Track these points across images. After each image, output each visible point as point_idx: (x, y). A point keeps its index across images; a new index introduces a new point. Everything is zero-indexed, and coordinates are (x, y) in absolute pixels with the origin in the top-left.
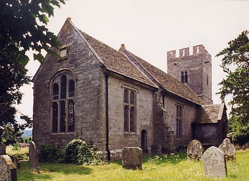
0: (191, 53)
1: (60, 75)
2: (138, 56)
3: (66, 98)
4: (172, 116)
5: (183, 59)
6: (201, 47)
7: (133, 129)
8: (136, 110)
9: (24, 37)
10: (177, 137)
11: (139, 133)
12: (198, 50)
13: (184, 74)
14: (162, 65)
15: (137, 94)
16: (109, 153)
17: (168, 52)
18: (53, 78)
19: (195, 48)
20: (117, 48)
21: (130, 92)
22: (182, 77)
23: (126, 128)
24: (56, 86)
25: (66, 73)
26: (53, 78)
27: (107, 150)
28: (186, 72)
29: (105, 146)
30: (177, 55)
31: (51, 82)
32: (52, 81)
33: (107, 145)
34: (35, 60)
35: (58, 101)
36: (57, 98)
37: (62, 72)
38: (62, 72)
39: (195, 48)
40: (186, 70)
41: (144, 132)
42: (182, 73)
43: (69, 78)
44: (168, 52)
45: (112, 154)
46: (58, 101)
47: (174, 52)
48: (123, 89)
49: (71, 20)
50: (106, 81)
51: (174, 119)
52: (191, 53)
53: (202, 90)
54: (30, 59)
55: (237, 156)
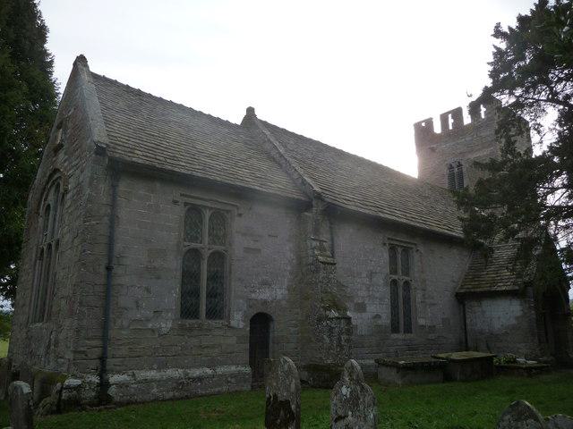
4: (371, 275)
9: (7, 277)
10: (395, 329)
11: (239, 320)
14: (406, 161)
15: (415, 253)
16: (104, 385)
17: (417, 126)
21: (400, 250)
23: (188, 311)
27: (102, 372)
28: (460, 165)
34: (250, 111)
39: (444, 118)
41: (260, 322)
45: (120, 385)
47: (429, 122)
48: (387, 247)
50: (114, 187)
51: (379, 280)
54: (412, 132)
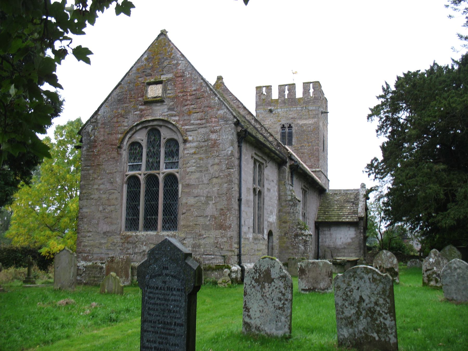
0: (299, 94)
1: (146, 127)
2: (135, 62)
3: (158, 168)
5: (284, 102)
6: (317, 85)
7: (260, 231)
8: (264, 196)
12: (312, 90)
13: (287, 130)
17: (257, 88)
18: (132, 132)
19: (306, 85)
20: (212, 81)
22: (283, 135)
24: (135, 145)
25: (161, 126)
26: (132, 132)
28: (290, 127)
29: (236, 257)
30: (275, 95)
31: (127, 139)
32: (129, 136)
33: (239, 255)
35: (142, 174)
36: (138, 167)
37: (151, 124)
38: (151, 124)
39: (306, 85)
40: (290, 122)
41: (270, 234)
42: (283, 127)
43: (165, 134)
44: (257, 88)
46: (142, 174)
49: (168, 34)
52: (299, 94)
53: (318, 160)
55: (254, 326)
